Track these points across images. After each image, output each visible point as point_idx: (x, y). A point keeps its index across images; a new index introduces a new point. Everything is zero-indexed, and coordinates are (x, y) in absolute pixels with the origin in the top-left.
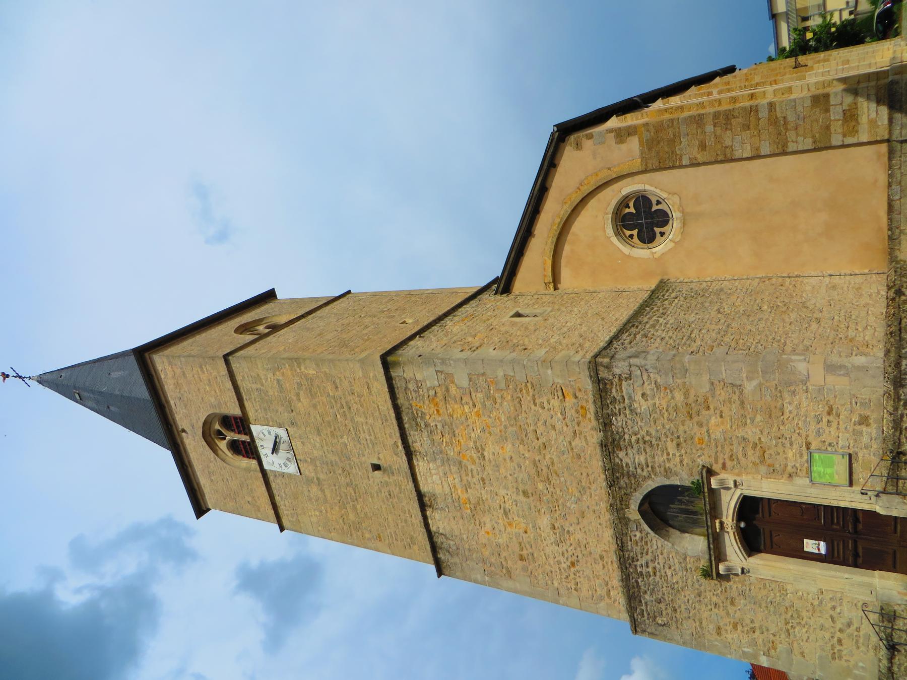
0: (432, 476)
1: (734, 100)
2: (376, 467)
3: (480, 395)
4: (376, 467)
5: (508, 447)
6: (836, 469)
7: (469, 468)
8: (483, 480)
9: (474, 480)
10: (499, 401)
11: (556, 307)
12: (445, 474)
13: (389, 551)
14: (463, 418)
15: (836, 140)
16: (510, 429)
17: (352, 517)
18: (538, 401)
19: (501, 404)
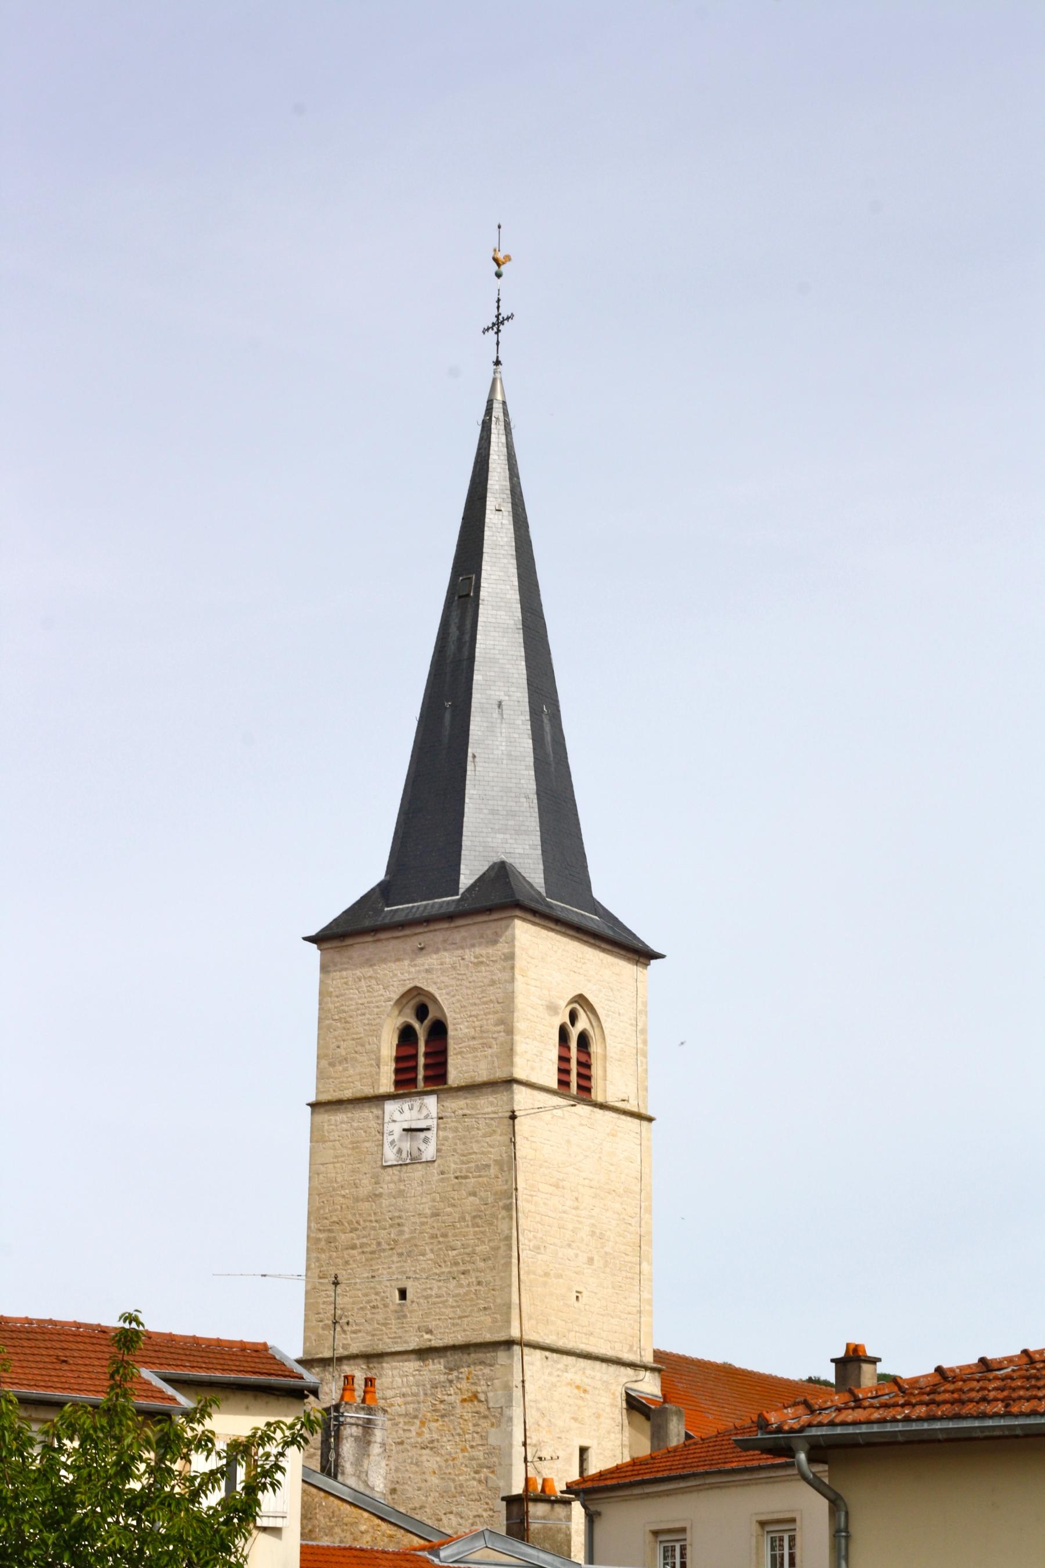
0: (401, 1377)
1: (481, 1370)
2: (403, 1294)
3: (481, 1455)
4: (403, 1294)
5: (434, 1480)
6: (626, 1348)
7: (412, 1428)
8: (402, 1443)
9: (401, 1432)
10: (477, 1476)
11: (555, 948)
12: (404, 1395)
13: (309, 1287)
14: (459, 1431)
15: (440, 1133)
16: (452, 1485)
17: (343, 1238)
18: (477, 1519)
19: (474, 1479)
